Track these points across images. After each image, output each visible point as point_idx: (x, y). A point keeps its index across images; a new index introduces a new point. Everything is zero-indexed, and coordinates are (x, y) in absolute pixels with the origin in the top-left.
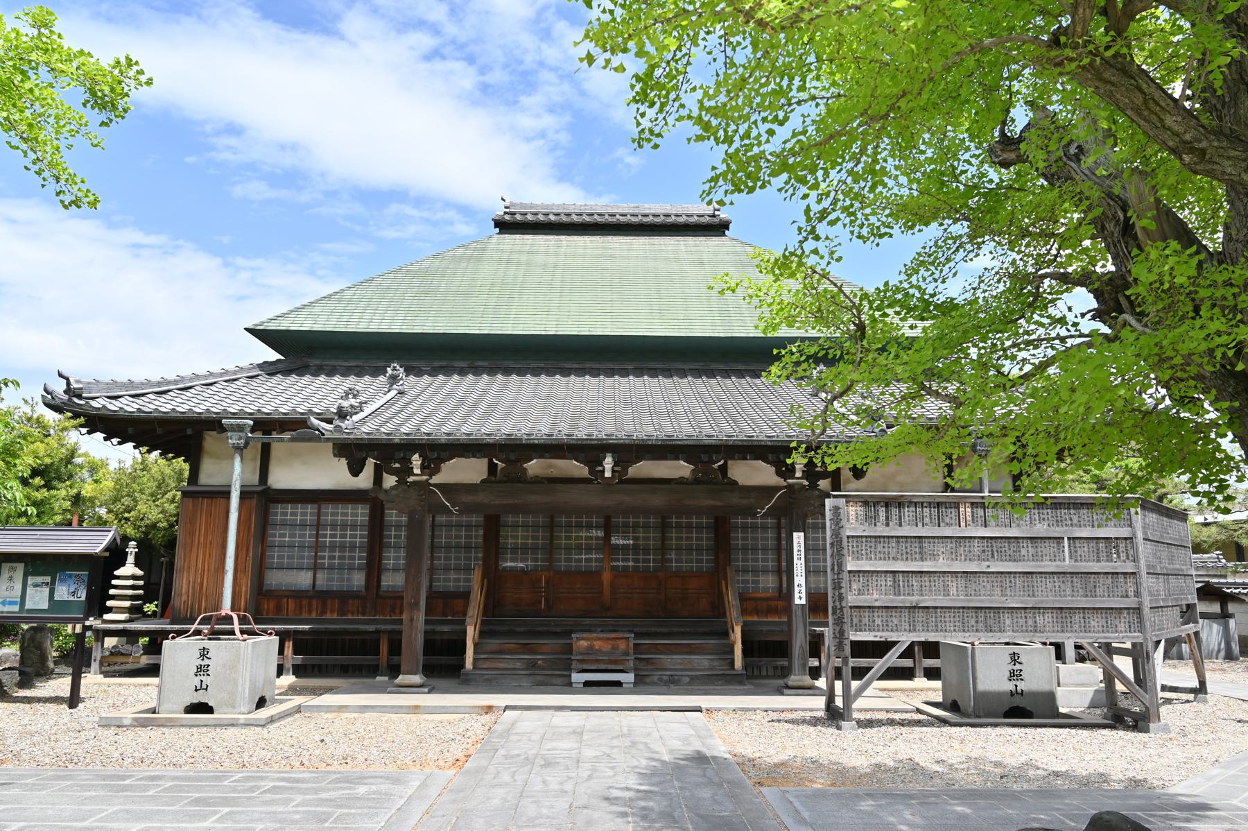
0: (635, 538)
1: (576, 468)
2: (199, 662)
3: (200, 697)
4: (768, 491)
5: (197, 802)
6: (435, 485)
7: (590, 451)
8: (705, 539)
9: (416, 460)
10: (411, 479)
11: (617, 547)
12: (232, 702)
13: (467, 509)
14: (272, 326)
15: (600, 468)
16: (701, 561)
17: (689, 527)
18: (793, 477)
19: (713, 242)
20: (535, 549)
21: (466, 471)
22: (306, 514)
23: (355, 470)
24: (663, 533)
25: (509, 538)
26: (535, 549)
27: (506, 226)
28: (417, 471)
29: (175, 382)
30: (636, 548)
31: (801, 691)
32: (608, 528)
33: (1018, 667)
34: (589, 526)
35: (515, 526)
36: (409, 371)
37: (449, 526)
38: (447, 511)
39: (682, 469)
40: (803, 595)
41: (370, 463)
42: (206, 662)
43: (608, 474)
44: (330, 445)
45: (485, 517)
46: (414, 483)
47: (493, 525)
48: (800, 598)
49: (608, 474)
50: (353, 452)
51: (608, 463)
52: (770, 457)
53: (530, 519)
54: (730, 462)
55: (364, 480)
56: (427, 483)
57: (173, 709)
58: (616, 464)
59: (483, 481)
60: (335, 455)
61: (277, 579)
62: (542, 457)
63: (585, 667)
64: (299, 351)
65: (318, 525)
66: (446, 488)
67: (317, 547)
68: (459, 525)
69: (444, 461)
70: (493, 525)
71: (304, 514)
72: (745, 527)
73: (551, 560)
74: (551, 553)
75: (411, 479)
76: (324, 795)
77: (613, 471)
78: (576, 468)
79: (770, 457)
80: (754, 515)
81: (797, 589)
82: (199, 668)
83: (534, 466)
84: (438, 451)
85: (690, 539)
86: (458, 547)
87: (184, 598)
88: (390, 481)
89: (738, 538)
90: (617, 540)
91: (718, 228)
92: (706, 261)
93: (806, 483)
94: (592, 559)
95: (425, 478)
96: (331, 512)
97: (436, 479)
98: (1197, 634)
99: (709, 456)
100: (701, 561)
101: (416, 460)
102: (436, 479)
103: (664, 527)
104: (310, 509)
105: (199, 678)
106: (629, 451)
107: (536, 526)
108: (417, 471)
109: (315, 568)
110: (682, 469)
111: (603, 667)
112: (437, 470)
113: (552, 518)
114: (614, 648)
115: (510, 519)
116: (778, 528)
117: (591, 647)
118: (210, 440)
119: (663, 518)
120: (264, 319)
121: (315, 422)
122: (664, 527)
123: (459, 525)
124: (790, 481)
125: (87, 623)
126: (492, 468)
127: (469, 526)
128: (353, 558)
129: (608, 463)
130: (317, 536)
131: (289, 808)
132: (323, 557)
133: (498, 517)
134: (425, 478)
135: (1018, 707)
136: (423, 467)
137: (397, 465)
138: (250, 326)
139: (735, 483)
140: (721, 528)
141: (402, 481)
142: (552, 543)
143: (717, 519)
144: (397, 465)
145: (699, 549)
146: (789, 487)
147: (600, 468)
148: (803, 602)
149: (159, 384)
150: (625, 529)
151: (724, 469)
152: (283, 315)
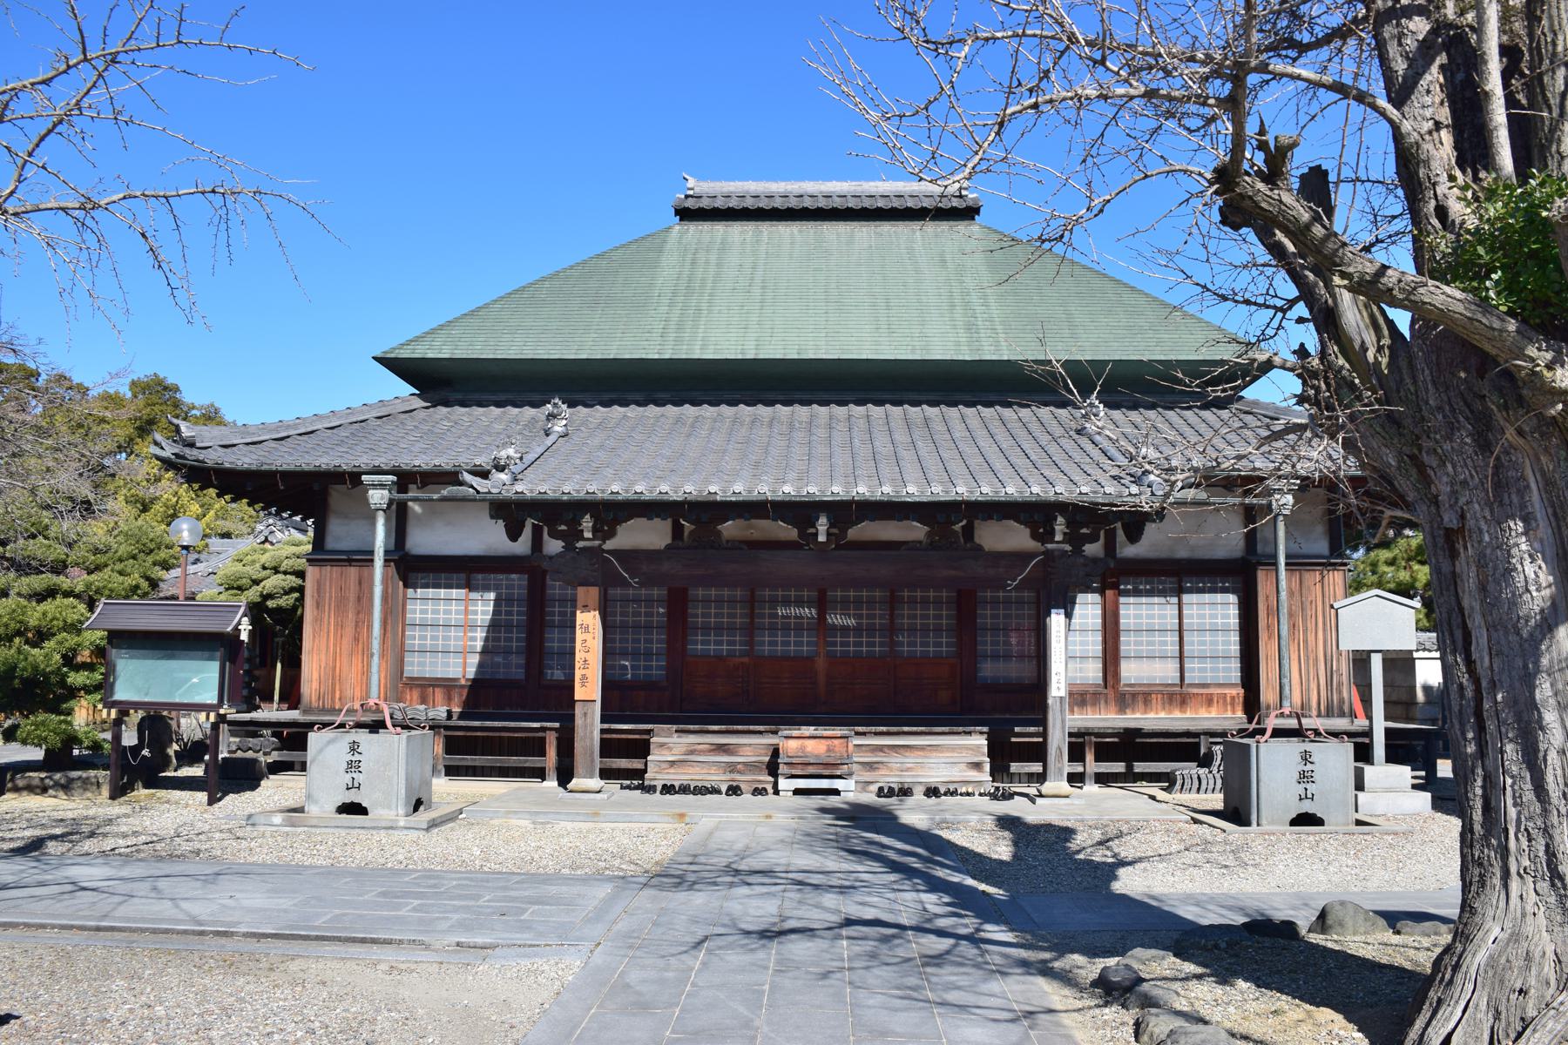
0: (859, 617)
1: (784, 531)
2: (349, 757)
3: (352, 797)
4: (1022, 557)
5: (384, 894)
6: (608, 552)
7: (800, 512)
8: (946, 617)
9: (587, 523)
10: (580, 544)
11: (834, 627)
12: (387, 805)
13: (648, 582)
14: (405, 354)
15: (812, 530)
16: (939, 644)
17: (925, 602)
18: (1052, 541)
19: (961, 227)
20: (773, 629)
21: (647, 535)
22: (704, 616)
23: (514, 535)
24: (892, 609)
25: (697, 615)
26: (731, 629)
27: (685, 214)
29: (295, 426)
30: (858, 630)
32: (822, 605)
33: (1309, 767)
34: (799, 603)
35: (707, 601)
36: (572, 405)
37: (626, 601)
38: (624, 584)
39: (916, 531)
40: (1063, 686)
41: (529, 522)
42: (357, 757)
43: (822, 538)
44: (487, 505)
45: (670, 590)
46: (584, 549)
47: (678, 603)
49: (822, 538)
50: (510, 512)
51: (822, 525)
52: (1022, 516)
53: (726, 592)
54: (977, 523)
55: (522, 546)
56: (600, 549)
57: (324, 805)
58: (832, 525)
59: (668, 547)
60: (492, 517)
61: (416, 667)
62: (740, 516)
63: (794, 772)
64: (439, 382)
66: (624, 555)
68: (637, 600)
69: (620, 523)
70: (678, 603)
72: (995, 602)
73: (751, 643)
74: (751, 635)
75: (580, 544)
76: (513, 893)
77: (829, 534)
78: (784, 531)
79: (1022, 516)
80: (1004, 587)
82: (350, 763)
83: (730, 528)
84: (611, 513)
85: (927, 617)
86: (637, 626)
88: (554, 546)
89: (985, 616)
90: (836, 619)
91: (969, 213)
92: (948, 257)
93: (1068, 548)
94: (804, 645)
95: (597, 543)
99: (944, 517)
100: (939, 644)
101: (587, 523)
103: (893, 602)
105: (349, 776)
106: (846, 512)
107: (732, 602)
110: (916, 531)
112: (611, 534)
113: (753, 592)
115: (700, 592)
116: (1038, 603)
117: (803, 748)
118: (337, 494)
119: (892, 592)
121: (468, 477)
122: (893, 602)
123: (637, 600)
124: (1049, 546)
125: (222, 711)
126: (677, 531)
127: (649, 601)
128: (510, 640)
129: (822, 525)
130: (466, 612)
131: (480, 903)
133: (685, 590)
134: (597, 543)
135: (1307, 814)
136: (595, 530)
137: (563, 527)
138: (378, 354)
139: (980, 548)
140: (965, 606)
141: (569, 547)
142: (752, 622)
143: (959, 592)
144: (563, 527)
145: (938, 630)
146: (1047, 553)
147: (812, 530)
148: (1062, 693)
149: (276, 430)
150: (844, 606)
151: (969, 532)
152: (416, 339)
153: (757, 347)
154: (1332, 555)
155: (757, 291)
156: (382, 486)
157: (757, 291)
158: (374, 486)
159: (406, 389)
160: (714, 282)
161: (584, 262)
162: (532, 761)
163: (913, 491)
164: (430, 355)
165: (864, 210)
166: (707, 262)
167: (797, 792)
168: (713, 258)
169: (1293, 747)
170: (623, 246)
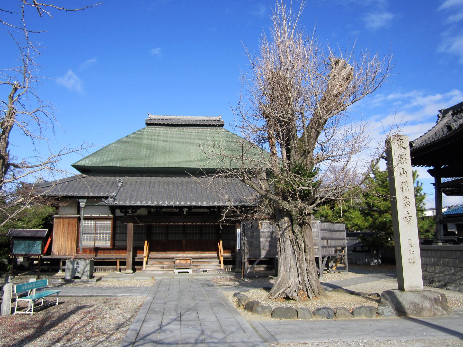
9: (130, 211)
10: (128, 214)
27: (148, 124)
28: (130, 212)
31: (176, 123)
46: (129, 216)
48: (307, 188)
56: (133, 216)
65: (96, 227)
67: (96, 233)
71: (91, 223)
75: (128, 214)
81: (238, 245)
83: (164, 210)
87: (56, 249)
91: (222, 126)
96: (99, 222)
97: (135, 214)
98: (77, 251)
102: (135, 214)
104: (93, 222)
108: (130, 212)
109: (95, 240)
111: (184, 268)
114: (187, 263)
117: (180, 262)
120: (76, 162)
130: (95, 230)
132: (97, 237)
138: (72, 164)
141: (125, 215)
152: (81, 160)
153: (167, 131)
154: (115, 248)
155: (168, 148)
156: (83, 202)
157: (168, 148)
158: (82, 202)
159: (78, 173)
160: (157, 145)
161: (123, 138)
162: (114, 267)
163: (205, 204)
164: (86, 165)
165: (195, 125)
166: (155, 139)
167: (179, 272)
168: (156, 138)
169: (91, 223)
170: (132, 134)
